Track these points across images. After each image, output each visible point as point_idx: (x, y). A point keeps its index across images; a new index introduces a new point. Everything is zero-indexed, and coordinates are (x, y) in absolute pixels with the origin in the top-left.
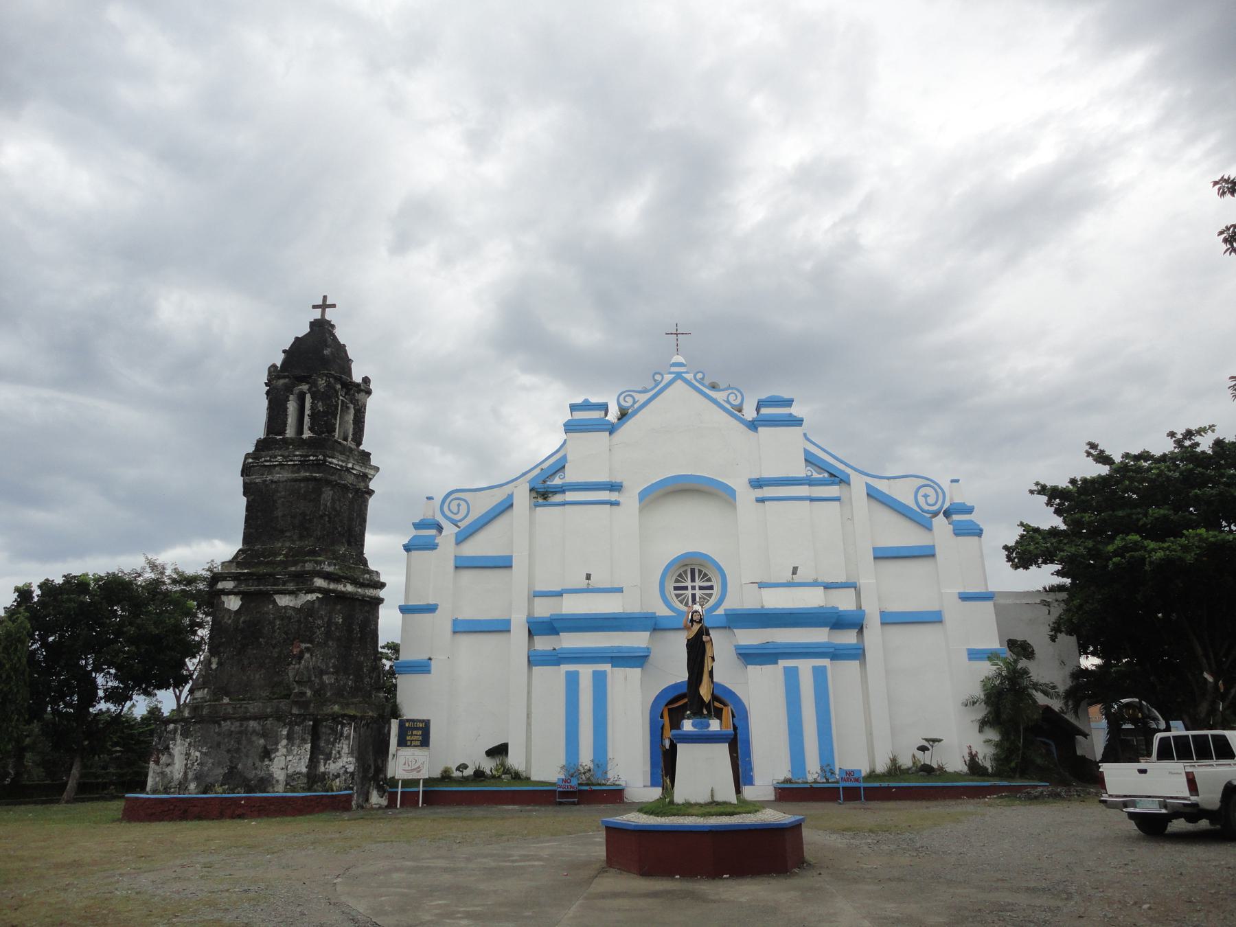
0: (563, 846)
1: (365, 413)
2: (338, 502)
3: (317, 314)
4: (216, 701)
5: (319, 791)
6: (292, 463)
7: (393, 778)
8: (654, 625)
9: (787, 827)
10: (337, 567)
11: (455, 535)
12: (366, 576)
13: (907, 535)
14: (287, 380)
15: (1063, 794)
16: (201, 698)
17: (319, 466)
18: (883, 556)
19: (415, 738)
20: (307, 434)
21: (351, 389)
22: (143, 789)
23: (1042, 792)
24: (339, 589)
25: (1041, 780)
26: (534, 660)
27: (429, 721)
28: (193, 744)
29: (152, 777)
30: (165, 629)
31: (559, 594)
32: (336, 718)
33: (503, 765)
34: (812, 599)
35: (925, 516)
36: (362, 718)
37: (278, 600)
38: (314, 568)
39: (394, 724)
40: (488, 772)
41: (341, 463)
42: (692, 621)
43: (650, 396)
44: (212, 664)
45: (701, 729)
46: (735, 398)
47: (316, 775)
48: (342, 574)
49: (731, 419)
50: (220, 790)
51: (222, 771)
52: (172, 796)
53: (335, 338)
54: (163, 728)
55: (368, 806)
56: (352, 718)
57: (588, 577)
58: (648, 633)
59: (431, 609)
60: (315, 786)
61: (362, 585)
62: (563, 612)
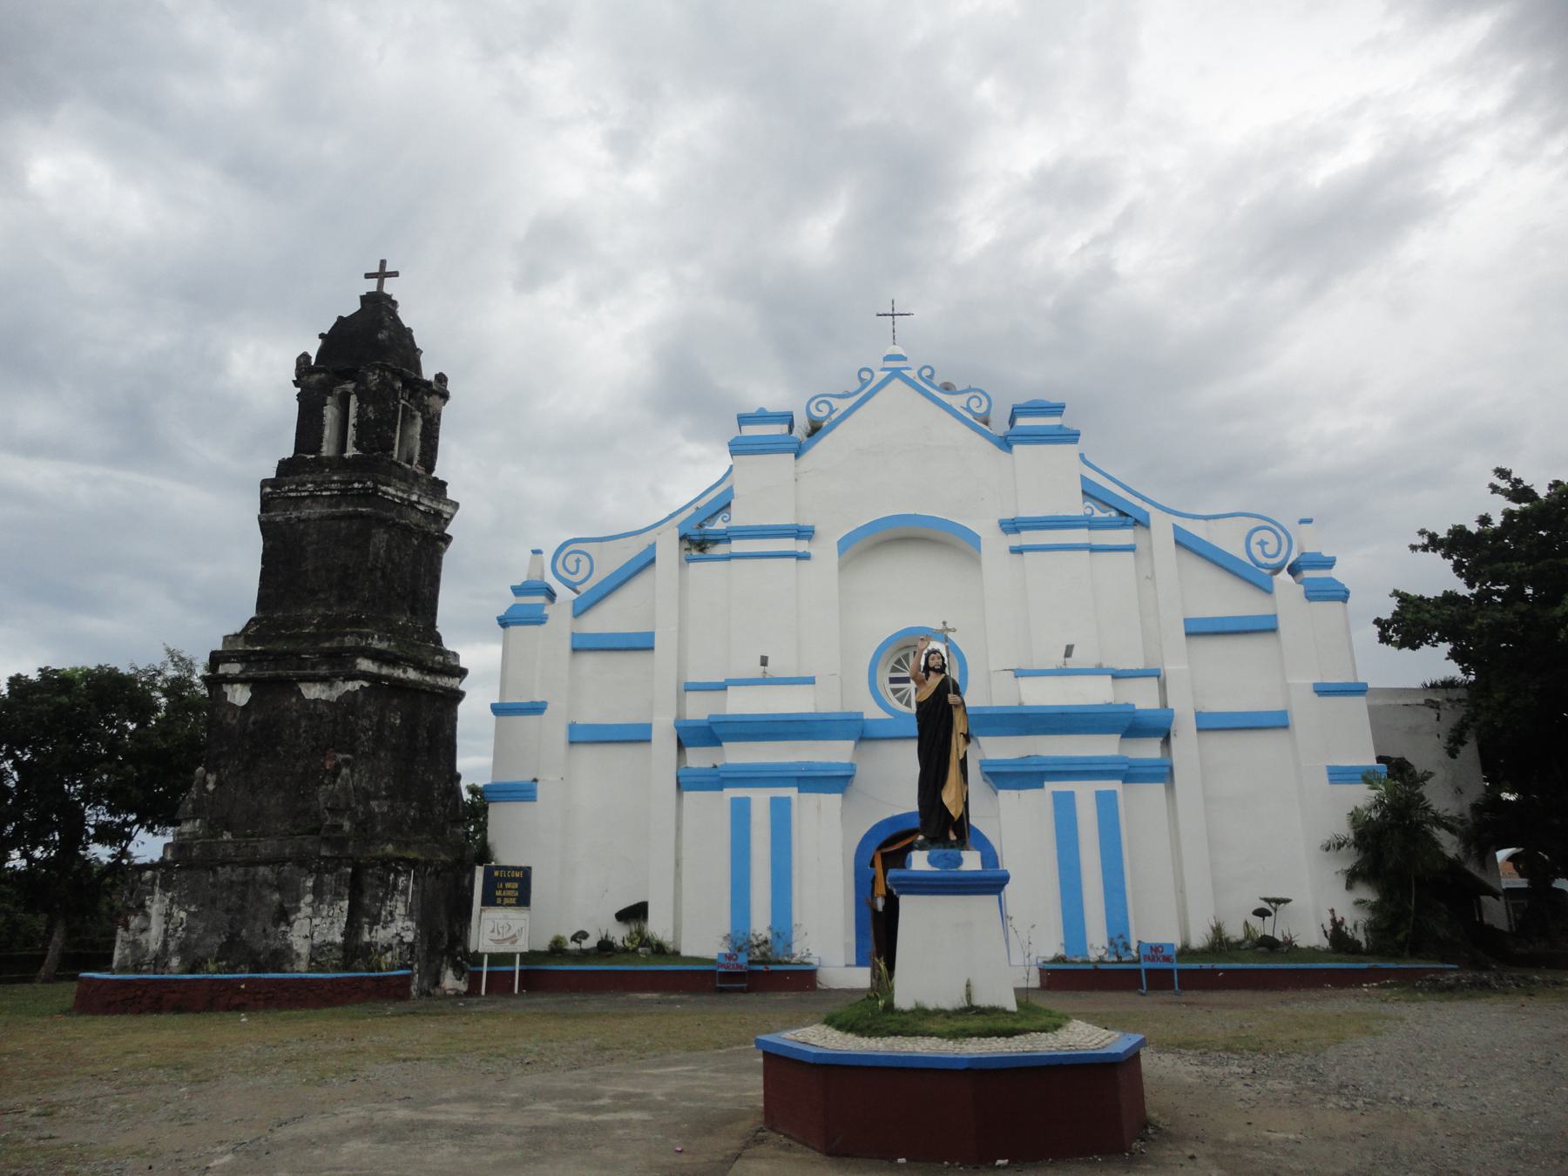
0: (700, 1074)
1: (439, 425)
2: (396, 552)
3: (371, 286)
4: (212, 837)
5: (362, 971)
6: (328, 493)
7: (477, 951)
8: (862, 732)
9: (1124, 1059)
10: (392, 644)
11: (571, 604)
12: (437, 658)
13: (1238, 602)
14: (323, 375)
15: (1493, 982)
16: (190, 833)
17: (368, 496)
18: (1197, 631)
19: (509, 893)
20: (351, 451)
21: (418, 390)
22: (108, 969)
23: (1458, 980)
24: (395, 675)
25: (1443, 960)
26: (686, 782)
27: (530, 868)
28: (176, 899)
29: (120, 948)
30: (176, 743)
31: (722, 687)
32: (387, 863)
33: (640, 933)
34: (1094, 693)
35: (1262, 572)
36: (427, 863)
37: (304, 691)
38: (357, 643)
39: (479, 872)
40: (620, 944)
41: (400, 494)
42: (927, 669)
43: (854, 402)
44: (207, 783)
45: (946, 867)
46: (978, 404)
47: (357, 947)
48: (400, 654)
49: (973, 434)
50: (212, 967)
51: (218, 940)
52: (144, 976)
53: (397, 320)
54: (136, 877)
55: (438, 991)
56: (412, 863)
57: (764, 661)
58: (852, 743)
59: (537, 709)
60: (356, 963)
61: (432, 671)
62: (728, 713)
